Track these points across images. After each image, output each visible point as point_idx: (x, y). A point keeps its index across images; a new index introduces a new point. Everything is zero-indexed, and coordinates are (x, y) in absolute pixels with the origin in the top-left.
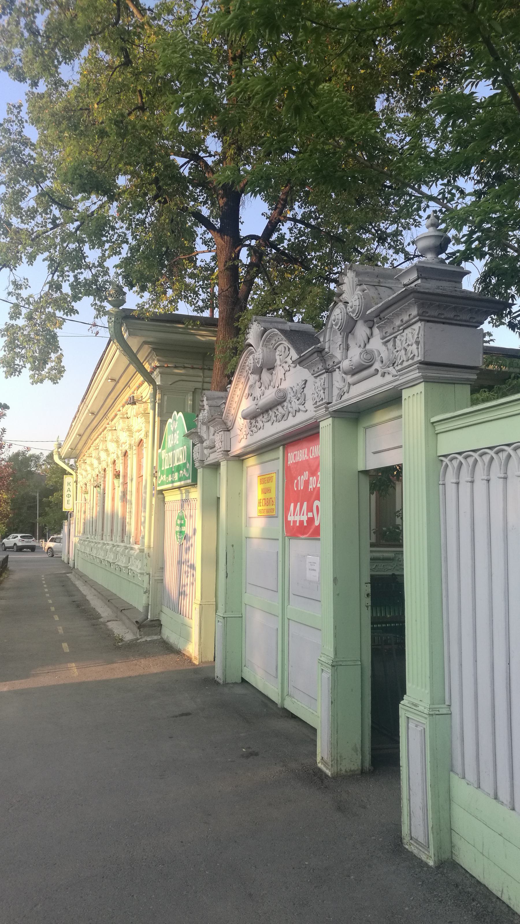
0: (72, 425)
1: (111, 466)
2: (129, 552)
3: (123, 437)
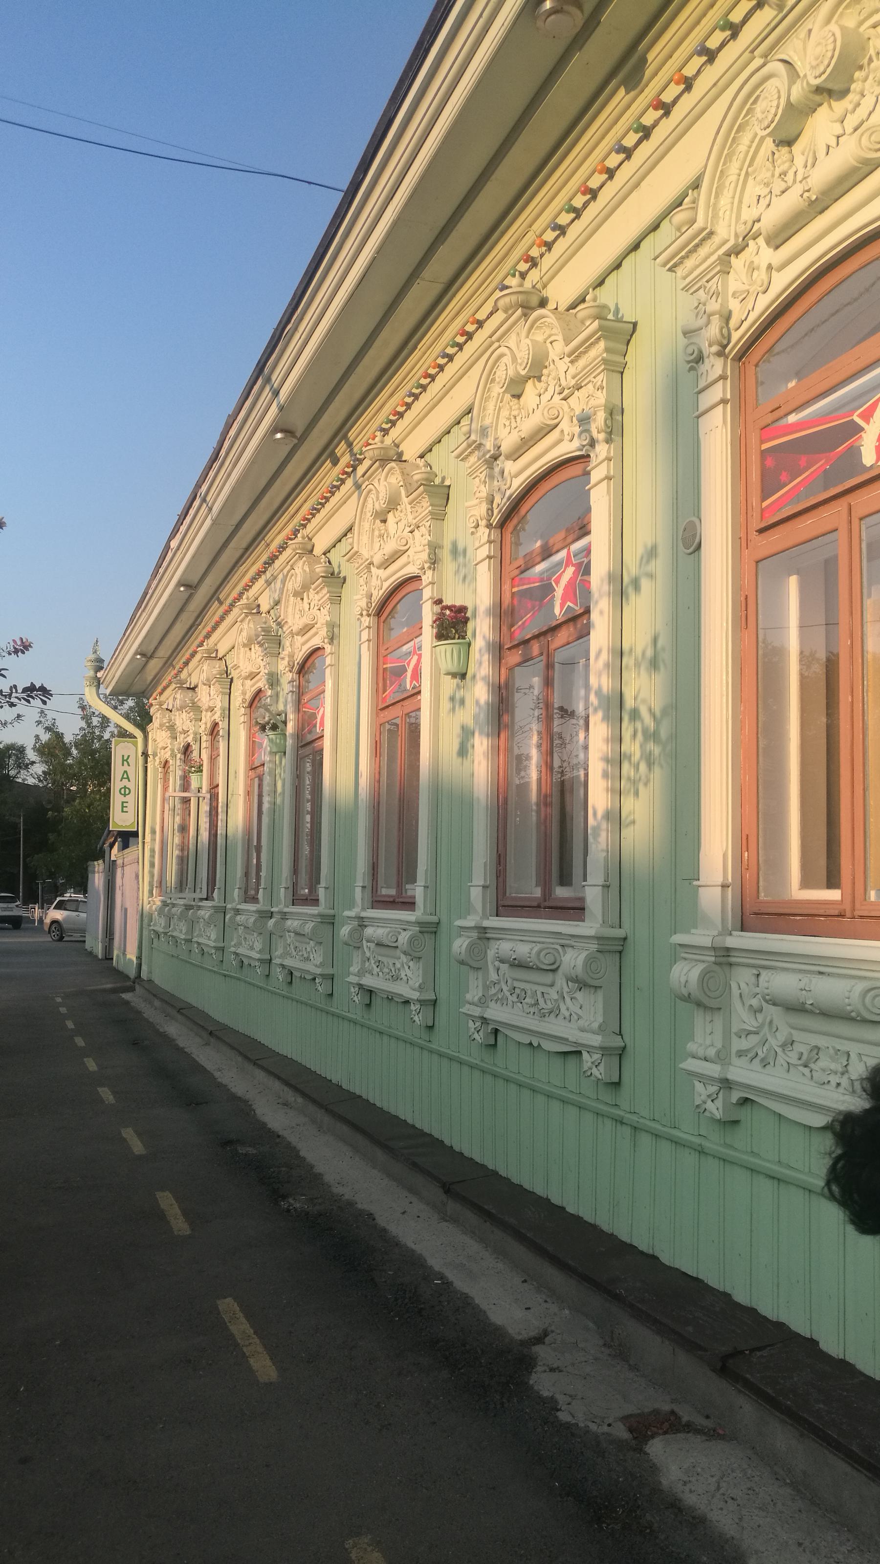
0: (167, 547)
1: (179, 756)
2: (170, 910)
3: (182, 720)
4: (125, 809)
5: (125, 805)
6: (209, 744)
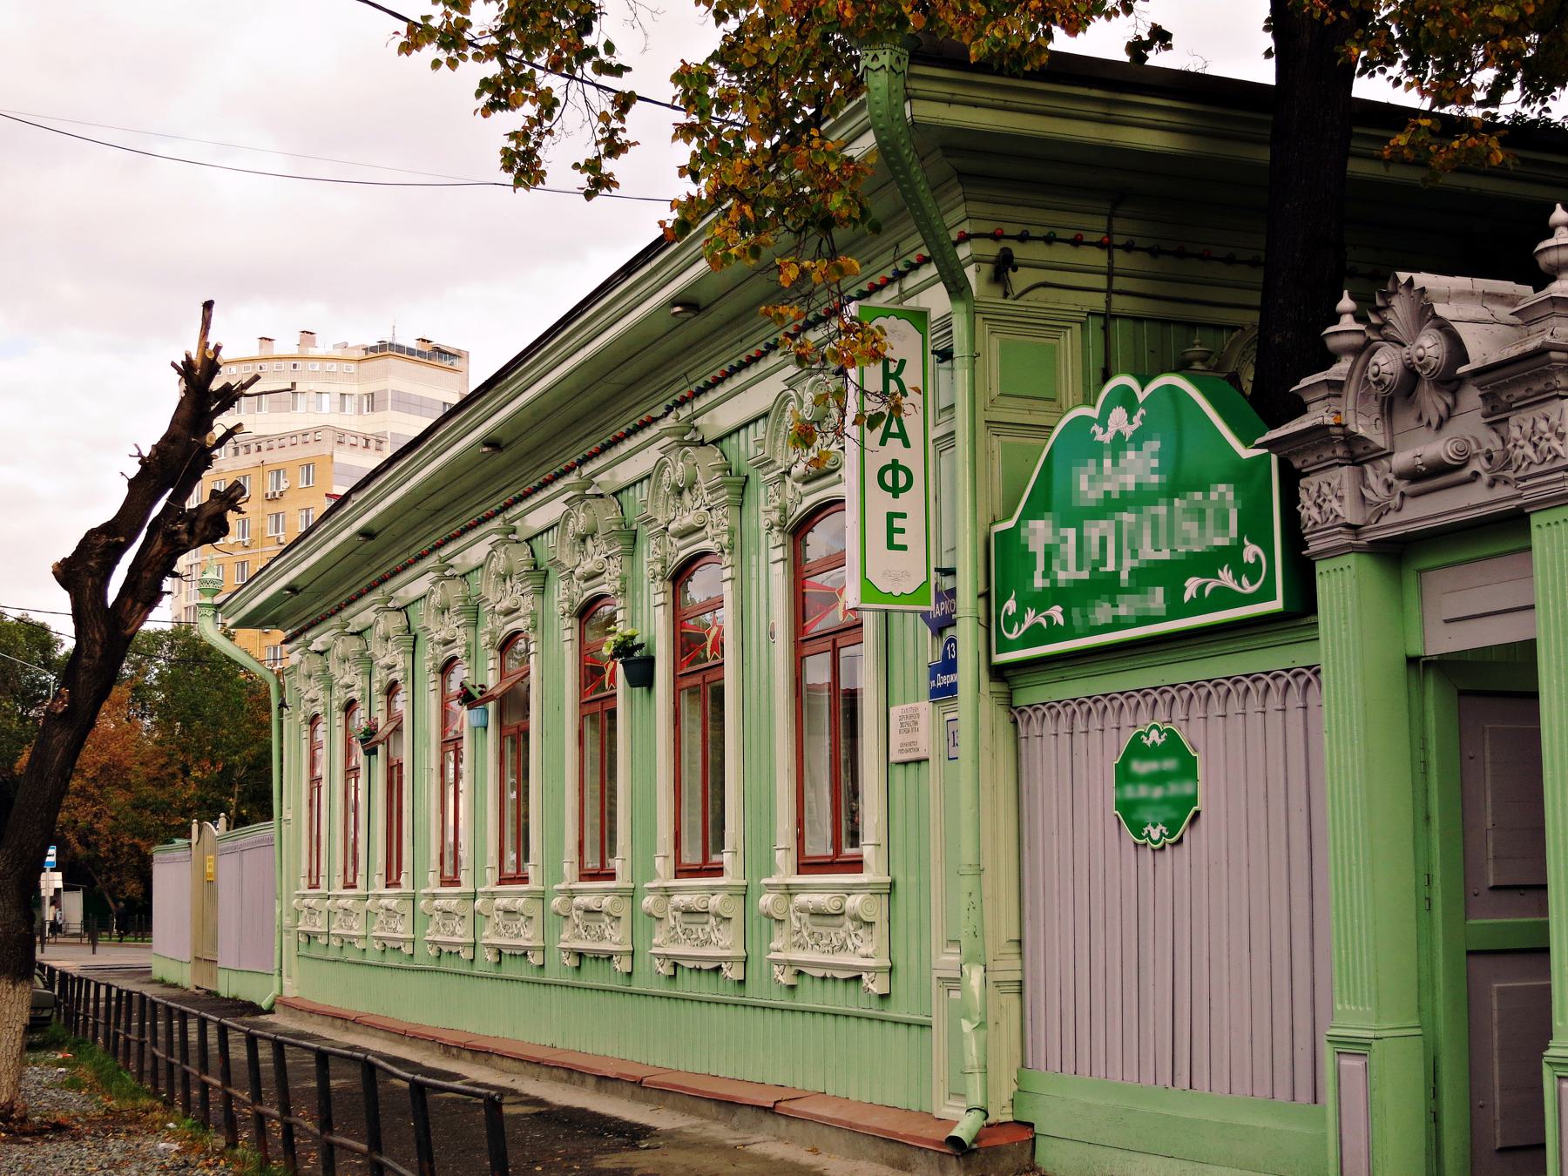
4: (898, 539)
5: (897, 523)
6: (384, 706)
